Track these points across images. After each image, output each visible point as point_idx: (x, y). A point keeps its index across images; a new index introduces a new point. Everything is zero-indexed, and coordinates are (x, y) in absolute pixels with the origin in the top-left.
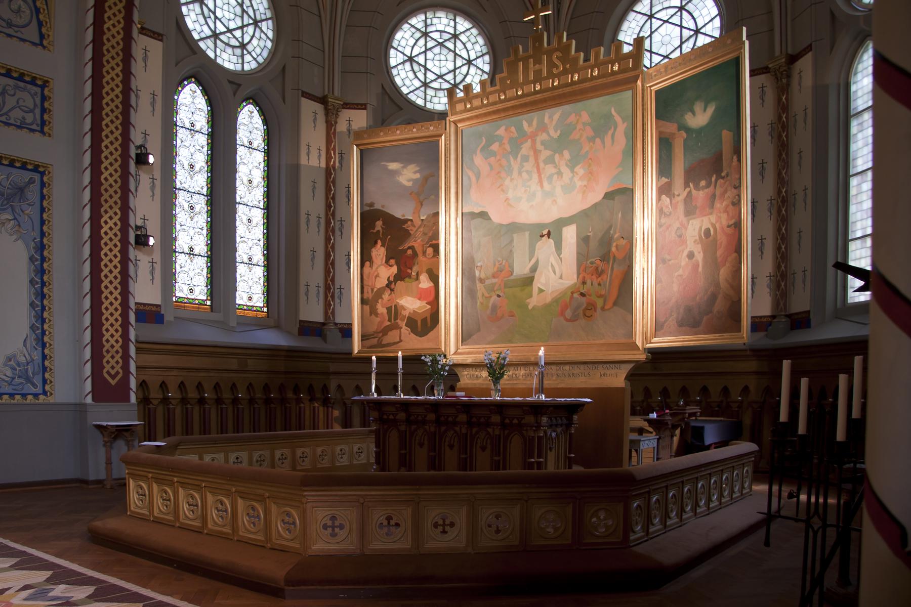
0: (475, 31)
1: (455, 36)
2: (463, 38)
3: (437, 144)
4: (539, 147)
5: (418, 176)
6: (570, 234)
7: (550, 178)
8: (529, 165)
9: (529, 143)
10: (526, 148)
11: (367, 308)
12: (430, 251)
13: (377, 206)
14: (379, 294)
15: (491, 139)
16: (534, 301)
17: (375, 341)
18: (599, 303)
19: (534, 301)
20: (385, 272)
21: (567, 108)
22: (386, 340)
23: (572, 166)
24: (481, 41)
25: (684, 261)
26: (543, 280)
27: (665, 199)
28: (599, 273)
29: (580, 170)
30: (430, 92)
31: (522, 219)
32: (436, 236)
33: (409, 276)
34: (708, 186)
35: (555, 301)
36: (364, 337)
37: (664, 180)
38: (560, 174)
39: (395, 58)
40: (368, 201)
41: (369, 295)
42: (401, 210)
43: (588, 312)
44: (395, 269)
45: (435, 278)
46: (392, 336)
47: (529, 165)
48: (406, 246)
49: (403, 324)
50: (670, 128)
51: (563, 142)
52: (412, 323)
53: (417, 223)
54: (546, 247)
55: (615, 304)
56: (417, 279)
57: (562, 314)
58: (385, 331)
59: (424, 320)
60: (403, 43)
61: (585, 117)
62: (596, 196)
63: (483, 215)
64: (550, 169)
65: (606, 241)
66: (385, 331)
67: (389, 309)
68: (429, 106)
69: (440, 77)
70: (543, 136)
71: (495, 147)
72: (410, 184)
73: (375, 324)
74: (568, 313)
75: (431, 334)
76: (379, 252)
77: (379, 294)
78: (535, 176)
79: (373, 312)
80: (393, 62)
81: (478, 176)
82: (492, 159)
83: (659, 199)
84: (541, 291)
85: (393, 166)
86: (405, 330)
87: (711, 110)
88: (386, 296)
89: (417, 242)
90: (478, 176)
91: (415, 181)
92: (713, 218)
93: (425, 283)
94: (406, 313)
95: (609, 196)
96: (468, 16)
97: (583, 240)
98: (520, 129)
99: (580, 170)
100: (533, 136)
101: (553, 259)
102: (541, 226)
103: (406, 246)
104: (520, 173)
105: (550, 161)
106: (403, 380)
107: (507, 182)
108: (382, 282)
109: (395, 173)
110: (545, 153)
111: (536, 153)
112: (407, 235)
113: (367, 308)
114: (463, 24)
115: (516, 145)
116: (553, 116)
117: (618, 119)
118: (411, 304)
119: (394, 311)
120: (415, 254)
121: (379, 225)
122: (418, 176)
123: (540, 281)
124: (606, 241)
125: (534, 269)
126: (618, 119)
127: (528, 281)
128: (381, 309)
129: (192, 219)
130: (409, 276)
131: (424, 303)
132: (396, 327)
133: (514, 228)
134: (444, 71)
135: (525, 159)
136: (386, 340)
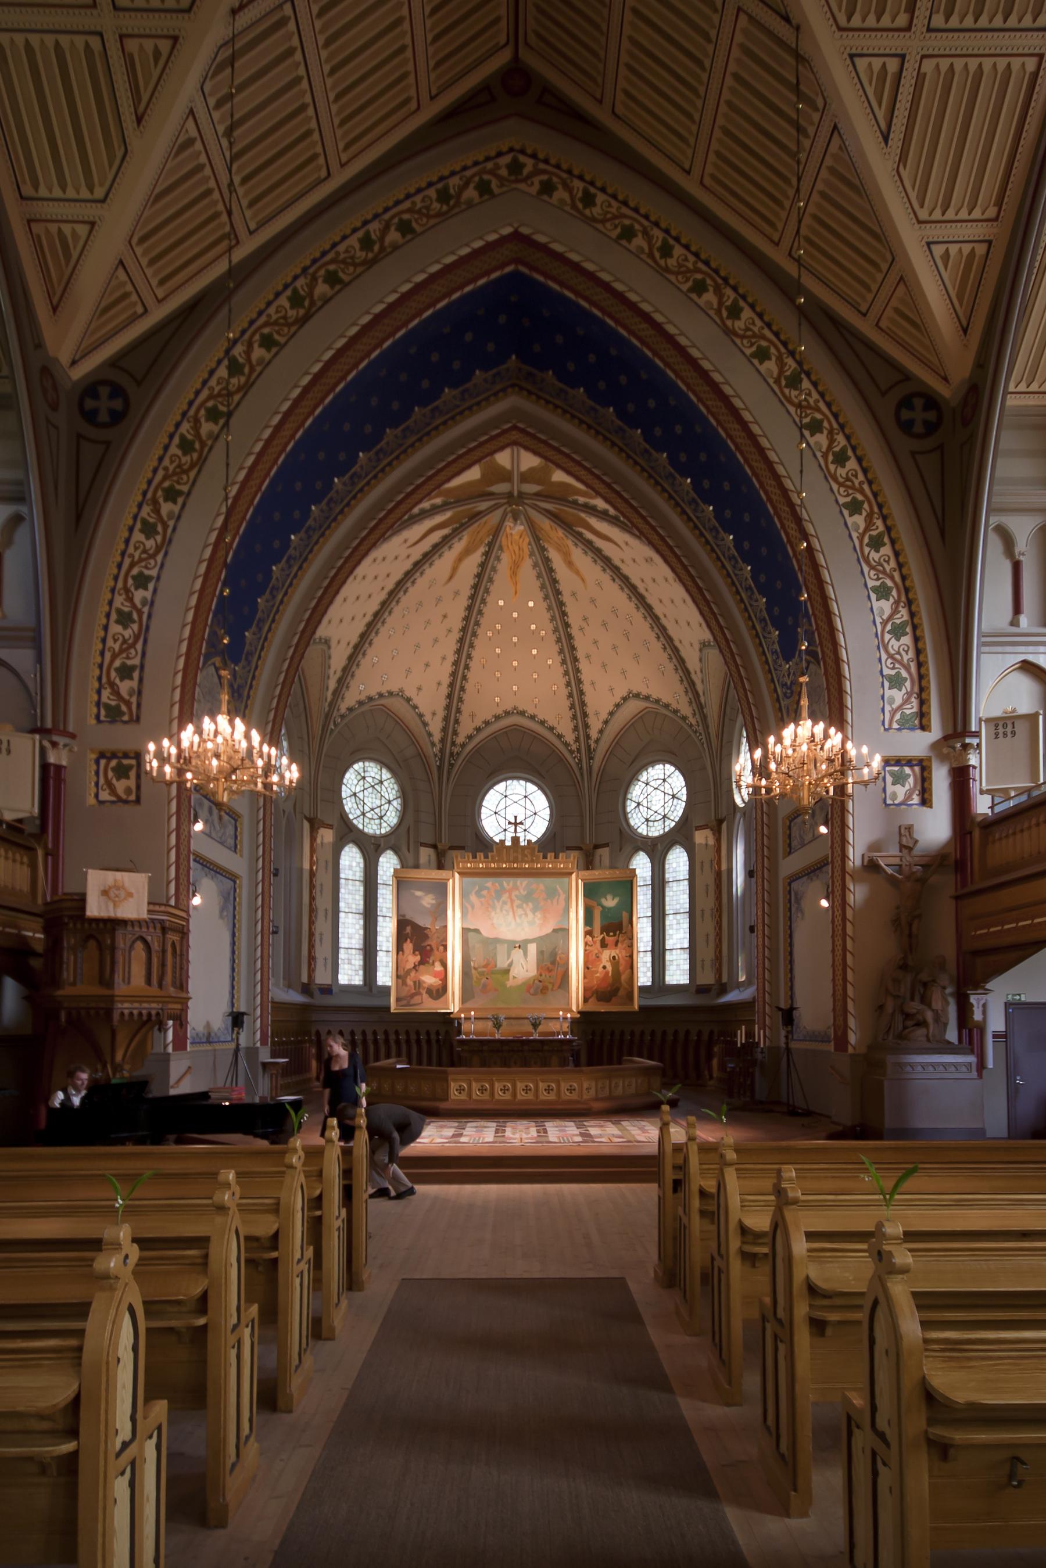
0: (393, 780)
1: (381, 782)
2: (385, 783)
3: (445, 886)
4: (514, 897)
5: (434, 902)
6: (532, 948)
7: (520, 916)
8: (507, 907)
9: (507, 895)
10: (505, 897)
11: (400, 981)
12: (441, 948)
13: (408, 917)
14: (408, 972)
15: (481, 889)
16: (510, 983)
17: (404, 1002)
18: (550, 986)
19: (510, 983)
20: (412, 959)
21: (531, 880)
22: (412, 1002)
23: (534, 911)
24: (396, 787)
25: (600, 969)
26: (516, 971)
27: (589, 938)
28: (549, 970)
29: (539, 915)
30: (367, 820)
31: (502, 936)
32: (445, 939)
33: (428, 962)
34: (615, 935)
35: (524, 984)
36: (398, 1000)
37: (588, 928)
38: (526, 915)
39: (345, 792)
40: (401, 913)
41: (401, 973)
42: (423, 921)
43: (544, 990)
44: (418, 958)
45: (444, 965)
46: (417, 999)
47: (507, 907)
48: (426, 944)
49: (424, 992)
50: (594, 903)
51: (527, 898)
52: (429, 991)
53: (434, 931)
54: (517, 955)
55: (559, 987)
56: (433, 964)
57: (528, 991)
58: (412, 996)
59: (438, 990)
60: (350, 782)
61: (542, 887)
62: (548, 930)
63: (477, 931)
64: (520, 911)
65: (554, 954)
66: (412, 996)
67: (415, 983)
68: (366, 830)
69: (372, 809)
70: (517, 893)
71: (485, 892)
72: (429, 906)
73: (405, 992)
74: (532, 991)
75: (442, 999)
76: (408, 946)
77: (408, 972)
78: (511, 913)
79: (404, 983)
80: (344, 795)
81: (473, 907)
82: (483, 899)
83: (585, 937)
84: (514, 977)
85: (418, 893)
86: (425, 996)
87: (616, 900)
88: (413, 974)
89: (433, 942)
90: (473, 907)
91: (432, 905)
92: (617, 951)
93: (438, 967)
94: (426, 985)
95: (555, 931)
96: (390, 769)
97: (540, 953)
98: (501, 885)
99: (539, 915)
100: (510, 891)
101: (522, 960)
102: (515, 942)
103: (426, 944)
104: (501, 910)
105: (520, 906)
106: (279, 1057)
107: (493, 914)
108: (410, 965)
109: (419, 898)
110: (517, 902)
111: (512, 901)
112: (427, 937)
113: (400, 981)
114: (386, 774)
115: (499, 894)
116: (523, 883)
117: (561, 891)
118: (429, 980)
119: (418, 984)
120: (432, 949)
121: (408, 929)
122: (434, 902)
123: (514, 972)
124: (554, 954)
125: (510, 965)
126: (561, 891)
127: (507, 971)
128: (410, 982)
129: (130, 895)
130: (428, 962)
131: (437, 980)
132: (418, 993)
133: (497, 941)
134: (375, 806)
135: (505, 903)
136: (412, 1002)
